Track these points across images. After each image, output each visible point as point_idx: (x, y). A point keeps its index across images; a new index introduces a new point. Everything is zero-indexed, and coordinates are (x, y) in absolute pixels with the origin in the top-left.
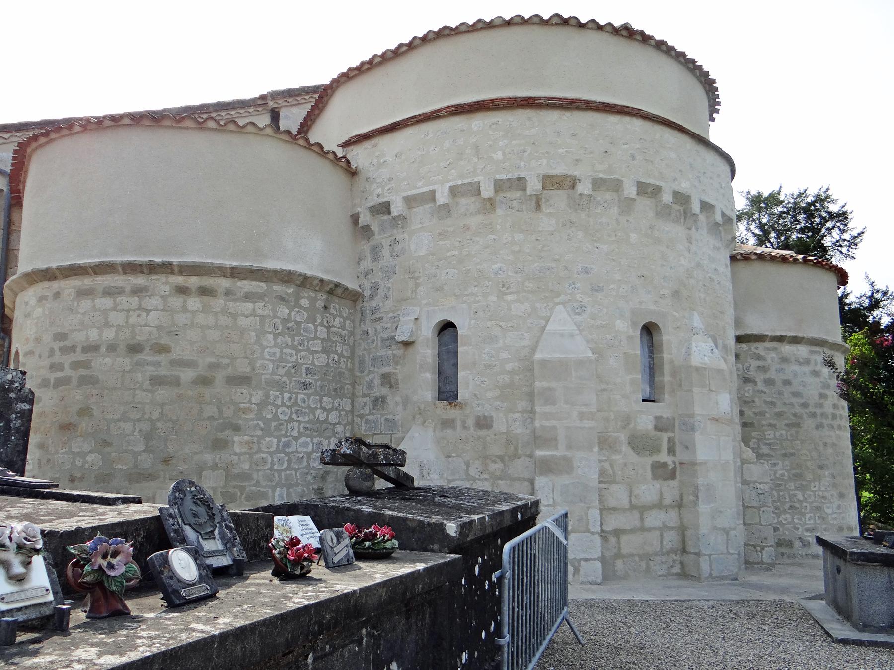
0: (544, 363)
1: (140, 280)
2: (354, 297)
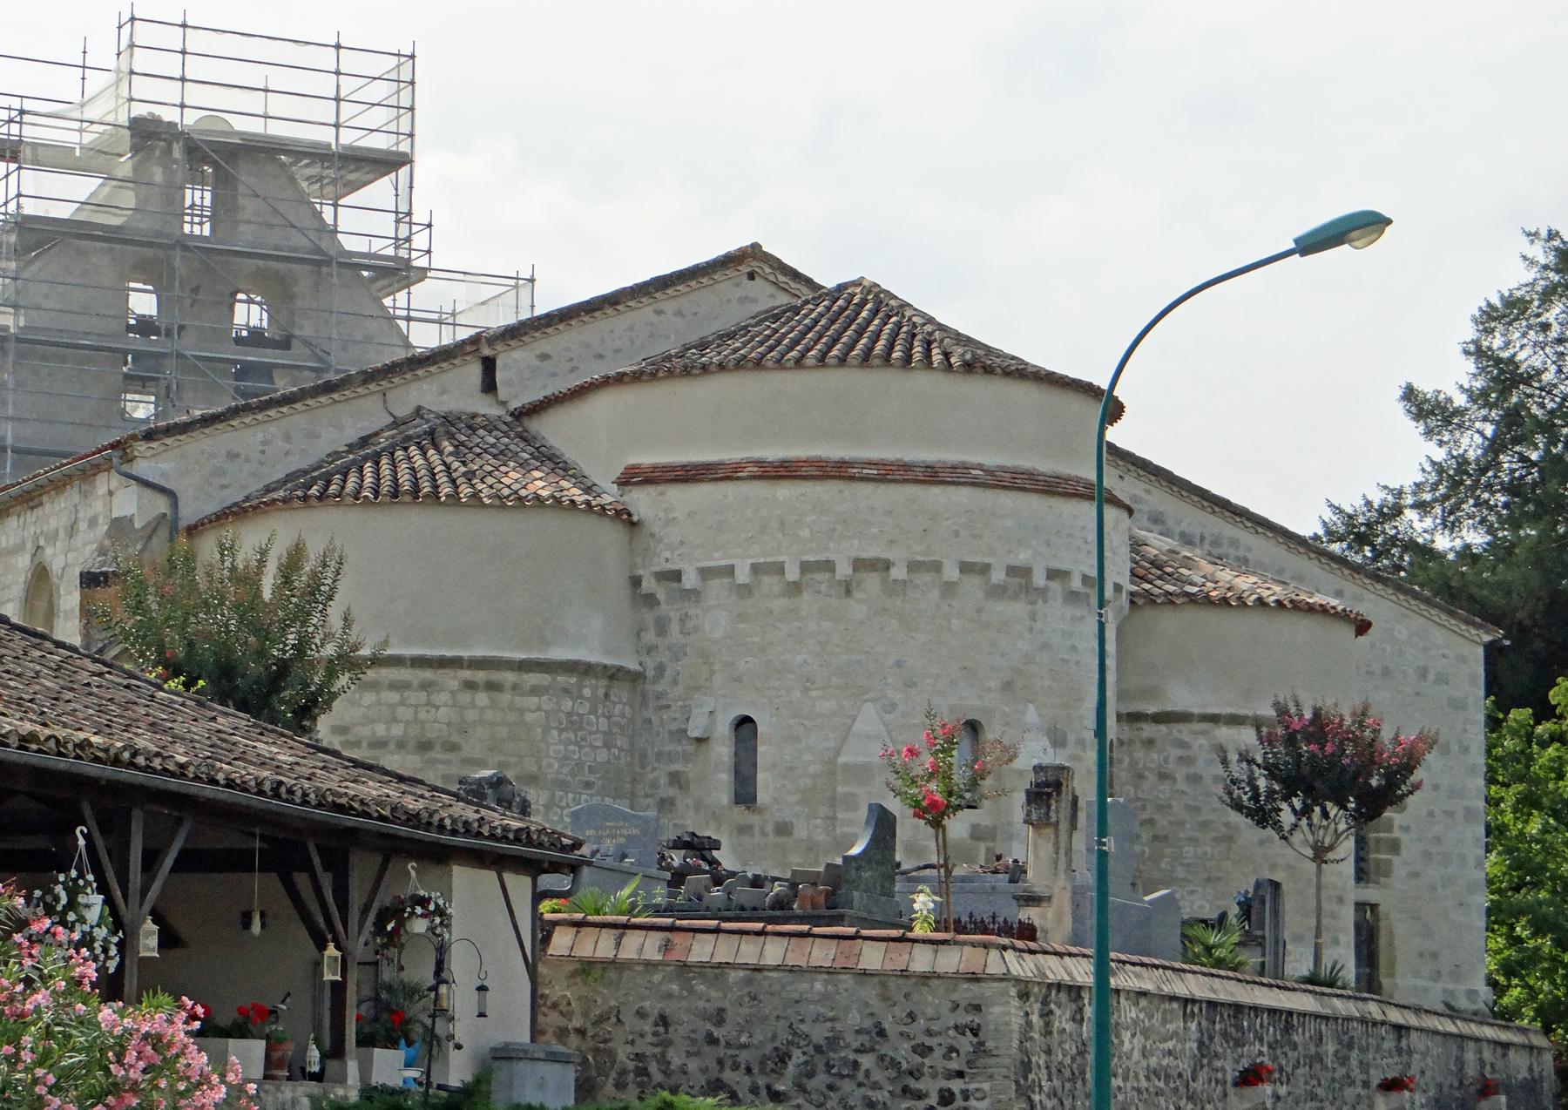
0: (847, 767)
1: (428, 674)
2: (635, 678)
